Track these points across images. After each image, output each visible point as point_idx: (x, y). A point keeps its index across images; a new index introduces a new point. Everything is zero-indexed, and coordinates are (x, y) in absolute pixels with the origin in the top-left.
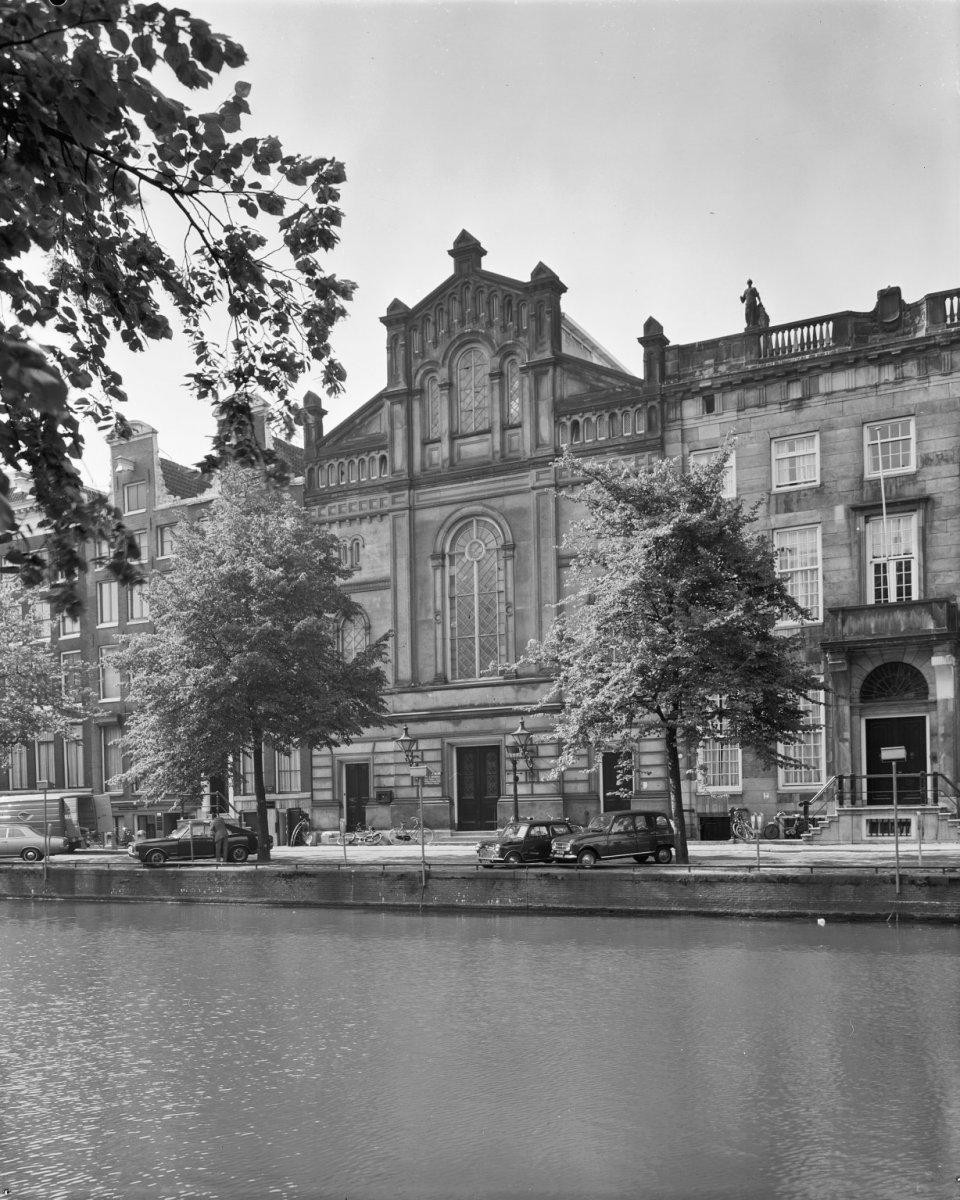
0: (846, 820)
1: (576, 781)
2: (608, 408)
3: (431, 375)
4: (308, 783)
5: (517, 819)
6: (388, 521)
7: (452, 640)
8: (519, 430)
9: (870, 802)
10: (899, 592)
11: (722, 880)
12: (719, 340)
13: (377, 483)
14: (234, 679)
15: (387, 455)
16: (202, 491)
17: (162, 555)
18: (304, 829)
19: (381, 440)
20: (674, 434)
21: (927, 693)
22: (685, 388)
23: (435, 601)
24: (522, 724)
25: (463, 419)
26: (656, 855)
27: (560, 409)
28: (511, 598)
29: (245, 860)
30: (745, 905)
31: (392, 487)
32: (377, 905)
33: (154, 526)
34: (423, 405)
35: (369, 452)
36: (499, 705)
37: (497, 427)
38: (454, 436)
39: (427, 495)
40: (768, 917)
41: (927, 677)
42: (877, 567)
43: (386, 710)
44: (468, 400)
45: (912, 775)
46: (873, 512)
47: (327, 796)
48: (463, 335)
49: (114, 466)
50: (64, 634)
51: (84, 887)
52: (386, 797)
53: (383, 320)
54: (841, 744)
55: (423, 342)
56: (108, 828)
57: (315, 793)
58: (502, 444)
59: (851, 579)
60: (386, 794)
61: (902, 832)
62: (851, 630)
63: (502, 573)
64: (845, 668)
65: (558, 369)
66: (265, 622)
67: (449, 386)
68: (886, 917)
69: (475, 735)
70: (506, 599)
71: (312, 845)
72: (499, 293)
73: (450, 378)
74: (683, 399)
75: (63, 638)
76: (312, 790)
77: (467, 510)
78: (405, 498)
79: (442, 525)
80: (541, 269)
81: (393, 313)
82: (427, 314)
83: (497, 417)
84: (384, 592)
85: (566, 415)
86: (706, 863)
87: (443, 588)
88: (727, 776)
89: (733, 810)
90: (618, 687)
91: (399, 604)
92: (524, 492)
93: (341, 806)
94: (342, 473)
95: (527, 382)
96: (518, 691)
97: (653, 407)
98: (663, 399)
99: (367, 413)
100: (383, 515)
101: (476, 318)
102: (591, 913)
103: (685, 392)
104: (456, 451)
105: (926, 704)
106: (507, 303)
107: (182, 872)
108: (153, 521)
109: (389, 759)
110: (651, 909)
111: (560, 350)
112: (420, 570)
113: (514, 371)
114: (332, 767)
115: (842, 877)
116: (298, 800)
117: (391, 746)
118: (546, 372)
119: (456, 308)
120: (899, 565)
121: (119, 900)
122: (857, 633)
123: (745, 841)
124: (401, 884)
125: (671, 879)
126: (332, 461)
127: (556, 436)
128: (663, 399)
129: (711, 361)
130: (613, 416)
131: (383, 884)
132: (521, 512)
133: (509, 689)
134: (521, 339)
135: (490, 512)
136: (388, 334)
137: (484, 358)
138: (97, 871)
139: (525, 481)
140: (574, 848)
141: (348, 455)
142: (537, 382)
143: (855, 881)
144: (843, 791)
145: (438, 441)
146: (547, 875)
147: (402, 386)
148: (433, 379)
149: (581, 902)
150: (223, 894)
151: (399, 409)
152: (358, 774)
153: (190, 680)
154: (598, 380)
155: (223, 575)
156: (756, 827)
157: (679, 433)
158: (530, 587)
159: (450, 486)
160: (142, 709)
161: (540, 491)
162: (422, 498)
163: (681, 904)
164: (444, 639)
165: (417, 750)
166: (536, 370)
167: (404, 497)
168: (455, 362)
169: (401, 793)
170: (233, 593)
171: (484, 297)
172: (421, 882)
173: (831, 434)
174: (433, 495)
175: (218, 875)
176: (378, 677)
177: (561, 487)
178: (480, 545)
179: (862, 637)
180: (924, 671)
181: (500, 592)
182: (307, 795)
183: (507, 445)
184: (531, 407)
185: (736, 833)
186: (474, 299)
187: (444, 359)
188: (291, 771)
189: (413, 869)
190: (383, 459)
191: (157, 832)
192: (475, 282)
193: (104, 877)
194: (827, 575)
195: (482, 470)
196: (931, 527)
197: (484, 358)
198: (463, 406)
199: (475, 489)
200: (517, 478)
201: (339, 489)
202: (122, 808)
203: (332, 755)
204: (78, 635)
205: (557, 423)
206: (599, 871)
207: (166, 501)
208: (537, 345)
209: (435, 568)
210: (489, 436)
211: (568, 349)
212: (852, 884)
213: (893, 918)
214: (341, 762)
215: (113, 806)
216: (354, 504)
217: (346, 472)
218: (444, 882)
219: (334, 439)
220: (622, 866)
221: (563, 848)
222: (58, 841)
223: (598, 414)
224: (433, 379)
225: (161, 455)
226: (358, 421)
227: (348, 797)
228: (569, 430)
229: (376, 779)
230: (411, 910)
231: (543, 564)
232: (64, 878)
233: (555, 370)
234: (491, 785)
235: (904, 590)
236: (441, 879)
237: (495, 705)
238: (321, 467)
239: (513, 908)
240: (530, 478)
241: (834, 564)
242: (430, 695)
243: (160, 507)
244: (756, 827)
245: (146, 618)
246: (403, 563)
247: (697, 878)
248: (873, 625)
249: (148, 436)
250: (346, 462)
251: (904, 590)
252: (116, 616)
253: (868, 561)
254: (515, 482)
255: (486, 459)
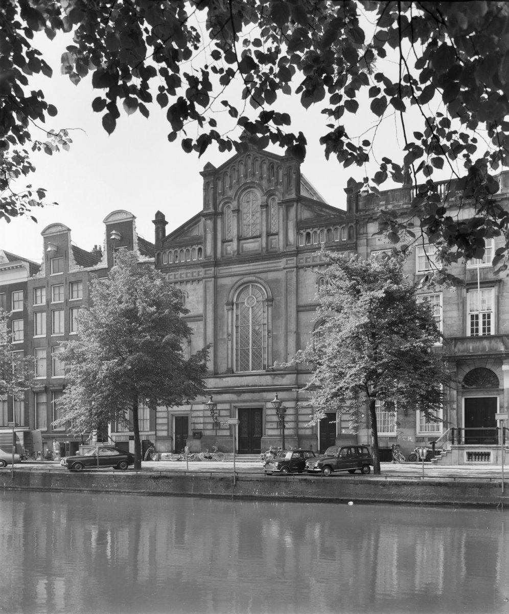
0: (456, 452)
1: (305, 428)
2: (326, 226)
3: (227, 205)
4: (154, 425)
5: (284, 448)
6: (202, 284)
7: (237, 350)
8: (277, 237)
9: (466, 443)
10: (484, 330)
11: (404, 484)
12: (388, 191)
13: (196, 263)
14: (130, 367)
15: (202, 248)
16: (96, 264)
17: (72, 298)
18: (151, 452)
19: (199, 239)
20: (363, 241)
21: (499, 385)
22: (369, 217)
23: (228, 329)
24: (277, 396)
25: (245, 229)
26: (362, 470)
27: (300, 226)
28: (270, 328)
29: (126, 469)
30: (418, 498)
31: (204, 265)
32: (207, 495)
33: (68, 282)
34: (223, 222)
35: (192, 246)
36: (263, 386)
37: (264, 235)
38: (240, 239)
39: (224, 270)
40: (431, 505)
41: (498, 376)
42: (472, 316)
43: (205, 387)
44: (248, 219)
45: (489, 428)
46: (471, 286)
47: (165, 434)
48: (246, 183)
49: (46, 248)
50: (14, 341)
51: (35, 482)
52: (198, 435)
54: (451, 411)
55: (224, 186)
56: (38, 448)
57: (157, 432)
58: (267, 243)
59: (458, 322)
60: (198, 433)
61: (482, 459)
62: (459, 350)
63: (266, 314)
64: (455, 370)
65: (299, 204)
66: (146, 336)
67: (238, 211)
68: (496, 505)
69: (248, 401)
70: (268, 328)
71: (156, 460)
72: (267, 162)
73: (239, 207)
74: (368, 222)
75: (14, 343)
76: (156, 430)
77: (246, 279)
78: (212, 272)
79: (233, 287)
81: (207, 170)
82: (226, 172)
83: (264, 229)
84: (199, 323)
85: (302, 229)
86: (390, 474)
87: (232, 321)
88: (388, 427)
89: (393, 446)
90: (352, 378)
91: (207, 329)
92: (279, 269)
93: (172, 439)
94: (177, 257)
95: (281, 211)
96: (273, 379)
97: (351, 226)
98: (357, 222)
99: (192, 224)
100: (199, 280)
101: (254, 175)
102: (330, 501)
103: (369, 219)
104: (241, 246)
105: (498, 391)
106: (271, 167)
107: (94, 475)
108: (67, 279)
109: (201, 414)
110: (364, 499)
111: (300, 193)
112: (219, 312)
113: (274, 204)
114: (168, 418)
115: (473, 483)
116: (148, 435)
117: (202, 407)
118: (293, 205)
119: (242, 168)
120: (484, 315)
121: (57, 491)
122: (462, 352)
123: (400, 463)
124: (221, 483)
125: (369, 482)
126: (171, 250)
127: (297, 241)
128: (357, 222)
129: (384, 203)
130: (329, 230)
131: (210, 483)
132: (277, 281)
133: (268, 377)
134: (279, 187)
135: (260, 280)
136: (204, 182)
137: (258, 196)
138: (43, 474)
139: (280, 264)
140: (320, 465)
141: (180, 247)
142: (287, 211)
143: (480, 486)
144: (454, 437)
145: (231, 241)
146: (305, 480)
147: (211, 210)
148: (229, 207)
149: (324, 495)
150: (117, 487)
151: (210, 223)
152: (182, 422)
153: (104, 367)
154: (321, 211)
155: (122, 310)
156: (423, 455)
157: (365, 240)
158: (281, 322)
159: (257, 263)
160: (73, 383)
161: (288, 270)
162: (221, 271)
163: (381, 496)
164: (232, 349)
165: (216, 410)
166: (287, 204)
167: (211, 271)
168: (241, 198)
169: (207, 433)
170: (127, 320)
171: (258, 164)
172: (233, 482)
174: (227, 271)
175: (115, 476)
176: (203, 368)
177: (300, 268)
178: (253, 298)
179: (465, 354)
180: (497, 372)
181: (264, 324)
182: (153, 433)
183: (269, 245)
184: (283, 225)
185: (395, 457)
186: (253, 164)
187: (235, 196)
189: (227, 475)
190: (200, 249)
191: (66, 452)
192: (254, 155)
193: (47, 477)
194: (445, 319)
195: (255, 257)
196: (502, 296)
197: (258, 196)
198: (245, 222)
199: (251, 267)
200: (275, 263)
201: (174, 265)
202: (48, 438)
203: (168, 411)
204: (22, 342)
205: (298, 233)
206: (333, 478)
207: (74, 268)
208: (288, 190)
209: (228, 310)
210: (259, 239)
211: (303, 193)
212: (478, 487)
213: (500, 506)
214: (172, 415)
215: (43, 437)
216: (183, 274)
217: (179, 256)
218: (246, 482)
219: (172, 237)
220: (343, 475)
221: (313, 464)
222: (17, 456)
223: (321, 229)
224: (229, 207)
225: (72, 243)
226: (186, 228)
227: (176, 434)
228: (197, 251)
229: (192, 425)
230: (227, 498)
231: (289, 310)
232: (22, 478)
233: (297, 205)
234: (257, 430)
235: (474, 330)
236: (245, 481)
237: (260, 386)
238: (165, 252)
239: (286, 498)
240: (282, 263)
241: (449, 314)
242: (224, 380)
243: (71, 271)
244: (423, 455)
245: (62, 333)
246: (210, 307)
247: (391, 483)
248: (471, 348)
249: (65, 232)
250: (179, 251)
251: (474, 330)
252: (44, 331)
253: (468, 313)
254: (275, 265)
255: (257, 252)
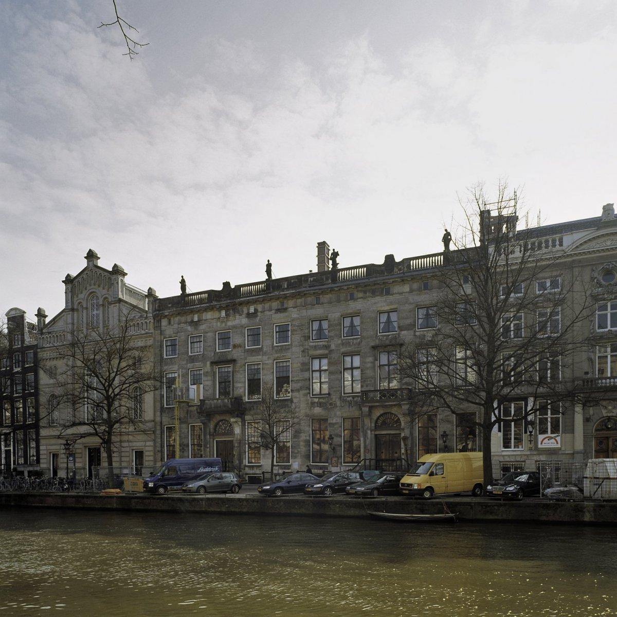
53: (63, 281)
57: (350, 371)
80: (115, 266)
173: (206, 334)
188: (568, 306)
